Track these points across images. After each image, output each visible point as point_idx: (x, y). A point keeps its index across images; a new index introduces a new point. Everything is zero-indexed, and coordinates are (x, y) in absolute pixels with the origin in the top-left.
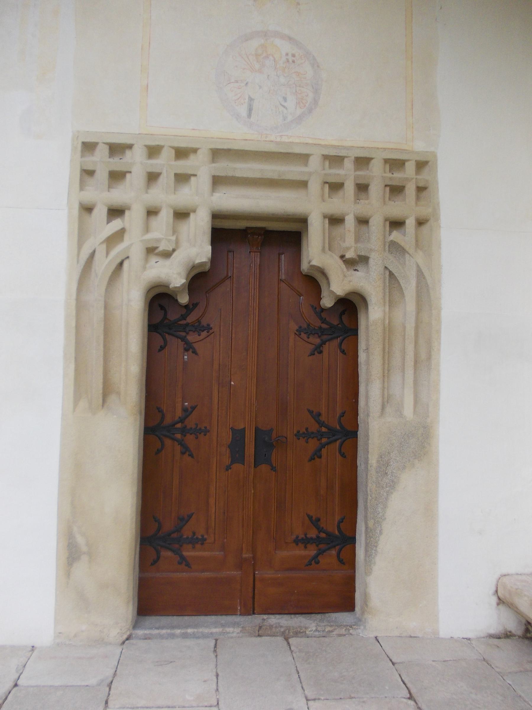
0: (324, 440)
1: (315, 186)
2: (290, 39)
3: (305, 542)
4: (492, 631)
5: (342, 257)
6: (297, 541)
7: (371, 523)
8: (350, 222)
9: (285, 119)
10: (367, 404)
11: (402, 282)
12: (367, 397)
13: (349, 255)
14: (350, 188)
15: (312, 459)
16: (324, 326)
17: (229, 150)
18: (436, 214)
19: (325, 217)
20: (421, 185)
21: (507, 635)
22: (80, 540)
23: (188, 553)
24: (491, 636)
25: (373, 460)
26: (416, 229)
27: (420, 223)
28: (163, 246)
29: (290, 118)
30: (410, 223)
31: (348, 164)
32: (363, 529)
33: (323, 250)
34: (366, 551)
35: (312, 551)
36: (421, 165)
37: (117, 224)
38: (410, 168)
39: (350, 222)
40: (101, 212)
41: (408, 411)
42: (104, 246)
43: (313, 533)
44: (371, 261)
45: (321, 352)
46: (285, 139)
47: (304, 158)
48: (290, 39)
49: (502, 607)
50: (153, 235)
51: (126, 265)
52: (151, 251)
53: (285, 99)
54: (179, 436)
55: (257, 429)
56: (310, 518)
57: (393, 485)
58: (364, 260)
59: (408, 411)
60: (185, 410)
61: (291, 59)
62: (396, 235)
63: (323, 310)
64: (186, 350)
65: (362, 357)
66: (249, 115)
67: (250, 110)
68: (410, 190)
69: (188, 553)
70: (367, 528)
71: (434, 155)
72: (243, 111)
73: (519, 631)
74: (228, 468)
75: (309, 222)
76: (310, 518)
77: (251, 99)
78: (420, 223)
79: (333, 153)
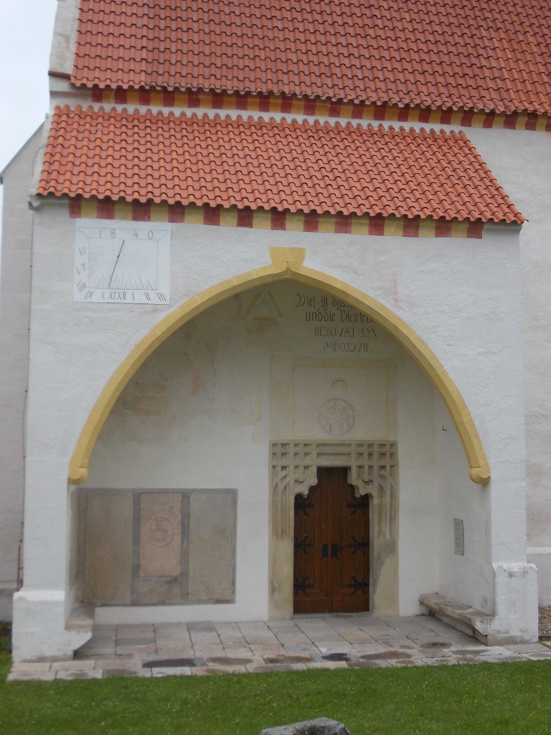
0: (357, 548)
1: (354, 455)
2: (344, 401)
3: (350, 586)
4: (418, 614)
5: (363, 481)
6: (347, 586)
7: (375, 577)
8: (366, 468)
9: (343, 431)
10: (373, 533)
11: (385, 489)
12: (373, 531)
13: (366, 480)
14: (366, 455)
15: (352, 555)
16: (356, 504)
17: (323, 444)
18: (397, 464)
19: (357, 466)
20: (392, 452)
21: (423, 615)
22: (276, 584)
23: (308, 591)
24: (417, 615)
25: (375, 554)
26: (390, 468)
27: (392, 466)
28: (301, 480)
29: (344, 431)
30: (388, 467)
31: (365, 447)
32: (372, 580)
33: (316, 335)
34: (373, 587)
35: (353, 589)
36: (392, 445)
37: (284, 473)
38: (388, 447)
39: (366, 468)
40: (279, 468)
41: (388, 536)
42: (280, 481)
43: (353, 583)
44: (374, 482)
45: (355, 514)
46: (343, 439)
47: (350, 445)
48: (344, 401)
49: (422, 605)
50: (297, 476)
51: (288, 487)
52: (296, 481)
53: (343, 424)
54: (303, 547)
55: (332, 545)
56: (352, 577)
57: (383, 563)
58: (371, 481)
59: (388, 536)
60: (305, 537)
61: (344, 408)
62: (382, 472)
63: (355, 497)
64: (305, 514)
65: (371, 516)
66: (330, 431)
67: (330, 429)
68: (388, 454)
69: (308, 591)
70: (373, 579)
71: (397, 442)
72: (328, 429)
73: (428, 614)
74: (321, 559)
75: (352, 468)
76: (352, 577)
77: (330, 424)
78: (392, 466)
79: (360, 443)
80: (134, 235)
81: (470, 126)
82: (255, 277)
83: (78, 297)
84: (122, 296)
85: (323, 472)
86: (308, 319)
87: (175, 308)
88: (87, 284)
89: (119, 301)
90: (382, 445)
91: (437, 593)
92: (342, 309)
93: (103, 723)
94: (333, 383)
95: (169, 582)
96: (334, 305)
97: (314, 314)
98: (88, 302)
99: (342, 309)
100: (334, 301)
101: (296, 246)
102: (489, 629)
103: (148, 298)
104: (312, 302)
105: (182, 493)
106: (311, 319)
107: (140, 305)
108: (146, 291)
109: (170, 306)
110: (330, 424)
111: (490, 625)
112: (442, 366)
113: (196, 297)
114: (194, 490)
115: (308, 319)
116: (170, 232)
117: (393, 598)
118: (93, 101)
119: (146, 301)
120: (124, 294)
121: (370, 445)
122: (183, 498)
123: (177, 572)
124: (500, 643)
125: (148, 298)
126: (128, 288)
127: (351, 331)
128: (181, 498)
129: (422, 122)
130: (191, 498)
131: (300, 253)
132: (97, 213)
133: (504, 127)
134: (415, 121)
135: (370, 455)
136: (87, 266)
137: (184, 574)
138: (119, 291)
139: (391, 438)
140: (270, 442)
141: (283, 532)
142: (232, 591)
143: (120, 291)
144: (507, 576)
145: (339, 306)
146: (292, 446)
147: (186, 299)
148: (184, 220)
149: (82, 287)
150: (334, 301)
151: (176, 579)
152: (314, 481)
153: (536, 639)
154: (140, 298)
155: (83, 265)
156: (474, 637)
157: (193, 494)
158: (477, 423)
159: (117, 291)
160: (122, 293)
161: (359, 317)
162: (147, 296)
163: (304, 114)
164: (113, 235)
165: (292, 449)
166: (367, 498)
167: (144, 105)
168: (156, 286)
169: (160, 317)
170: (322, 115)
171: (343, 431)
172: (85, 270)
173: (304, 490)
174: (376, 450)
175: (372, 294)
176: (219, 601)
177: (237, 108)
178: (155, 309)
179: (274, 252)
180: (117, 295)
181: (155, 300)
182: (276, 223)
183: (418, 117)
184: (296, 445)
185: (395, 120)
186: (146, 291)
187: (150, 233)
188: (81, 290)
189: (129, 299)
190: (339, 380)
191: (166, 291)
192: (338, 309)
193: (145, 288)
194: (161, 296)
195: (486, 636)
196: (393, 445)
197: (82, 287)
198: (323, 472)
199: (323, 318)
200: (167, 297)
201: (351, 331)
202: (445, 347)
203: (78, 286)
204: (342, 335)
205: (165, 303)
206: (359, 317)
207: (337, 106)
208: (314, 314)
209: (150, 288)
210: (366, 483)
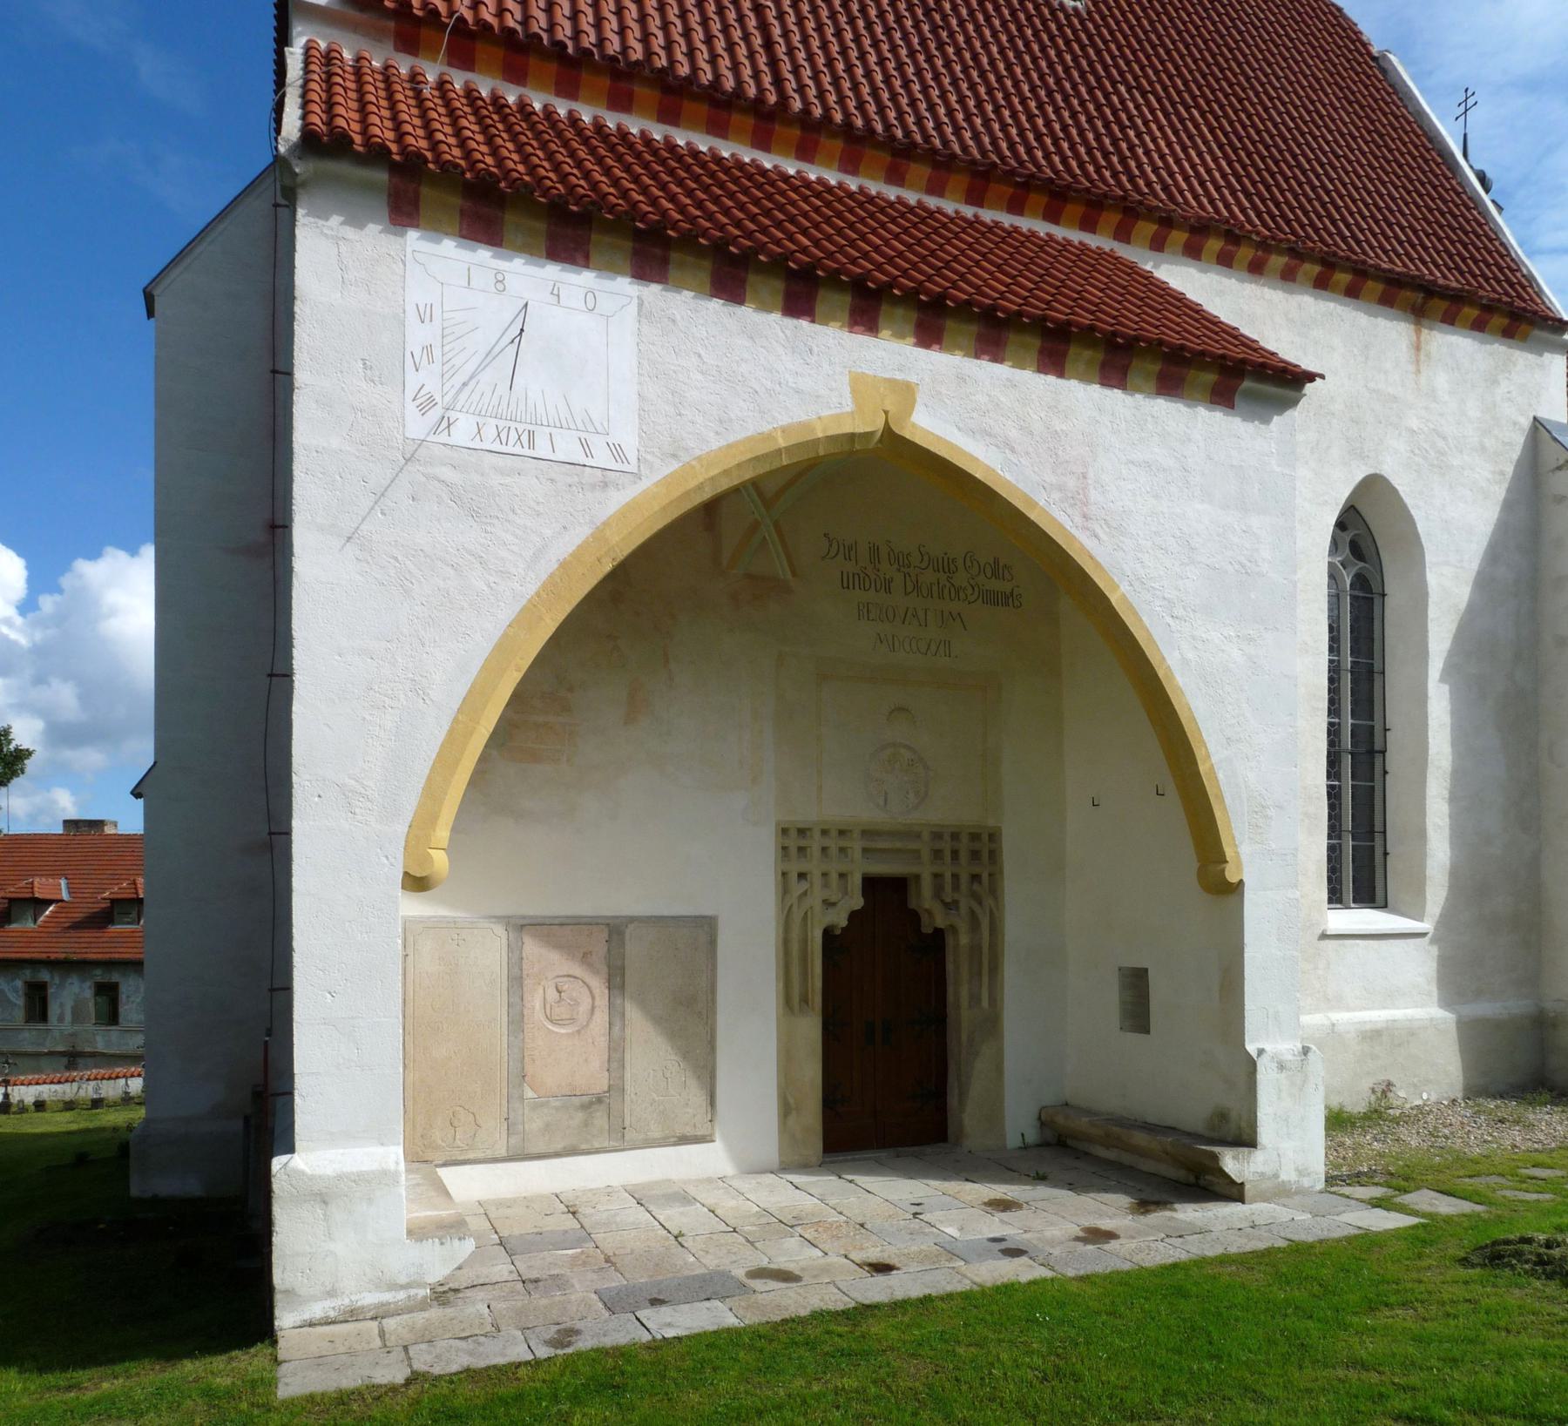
22: (791, 1101)
25: (964, 1037)
37: (804, 886)
41: (985, 1003)
47: (918, 836)
53: (908, 793)
59: (985, 1003)
62: (976, 887)
65: (950, 967)
67: (886, 800)
71: (1000, 828)
72: (881, 803)
80: (552, 293)
81: (1128, 242)
82: (820, 435)
83: (417, 426)
84: (525, 438)
85: (872, 884)
86: (845, 585)
87: (646, 483)
88: (438, 399)
89: (517, 450)
90: (975, 837)
91: (1067, 1104)
92: (906, 570)
93: (171, 1228)
94: (891, 713)
95: (585, 1107)
96: (892, 562)
97: (856, 577)
98: (444, 445)
99: (906, 570)
100: (892, 554)
101: (899, 376)
102: (1246, 1172)
103: (588, 451)
104: (853, 553)
105: (608, 925)
106: (851, 586)
107: (568, 466)
108: (583, 435)
109: (637, 476)
110: (886, 793)
111: (1248, 1162)
112: (1164, 658)
113: (694, 463)
114: (632, 919)
115: (845, 585)
116: (635, 301)
117: (994, 1118)
118: (397, 49)
119: (582, 459)
120: (531, 434)
121: (955, 836)
122: (610, 935)
123: (601, 1084)
124: (1265, 1197)
125: (588, 451)
126: (133, 891)
127: (921, 614)
128: (605, 935)
129: (1049, 221)
130: (627, 937)
131: (906, 392)
132: (461, 224)
133: (1184, 254)
134: (1036, 218)
135: (955, 854)
136: (437, 352)
137: (617, 1088)
138: (517, 425)
139: (991, 822)
140: (777, 824)
141: (805, 1000)
142: (709, 1118)
143: (521, 428)
144: (1276, 1069)
145: (901, 563)
146: (817, 834)
147: (674, 466)
148: (667, 279)
149: (427, 404)
150: (892, 554)
151: (599, 1100)
152: (857, 902)
153: (1321, 1185)
154: (568, 448)
155: (428, 349)
156: (1198, 1186)
157: (631, 927)
158: (1221, 776)
159: (513, 425)
160: (526, 432)
161: (935, 588)
162: (585, 445)
163: (839, 170)
164: (500, 287)
165: (816, 841)
166: (939, 934)
167: (512, 83)
168: (606, 426)
169: (616, 500)
170: (873, 178)
171: (907, 806)
172: (431, 361)
173: (840, 919)
174: (964, 845)
175: (1041, 499)
176: (684, 1140)
177: (708, 133)
178: (606, 481)
179: (859, 384)
180: (513, 435)
181: (602, 458)
182: (859, 319)
183: (1041, 211)
184: (824, 832)
185: (1002, 210)
186: (583, 435)
187: (590, 296)
188: (423, 409)
189: (542, 449)
190: (901, 709)
191: (631, 444)
192: (899, 570)
193: (581, 426)
194: (617, 451)
195: (1242, 1184)
196: (994, 836)
197: (427, 404)
198: (872, 884)
199: (873, 585)
200: (632, 457)
201: (921, 614)
202: (1169, 620)
203: (414, 400)
204: (906, 622)
205: (625, 467)
206: (935, 588)
207: (904, 162)
208: (856, 577)
209: (591, 429)
210: (947, 905)
